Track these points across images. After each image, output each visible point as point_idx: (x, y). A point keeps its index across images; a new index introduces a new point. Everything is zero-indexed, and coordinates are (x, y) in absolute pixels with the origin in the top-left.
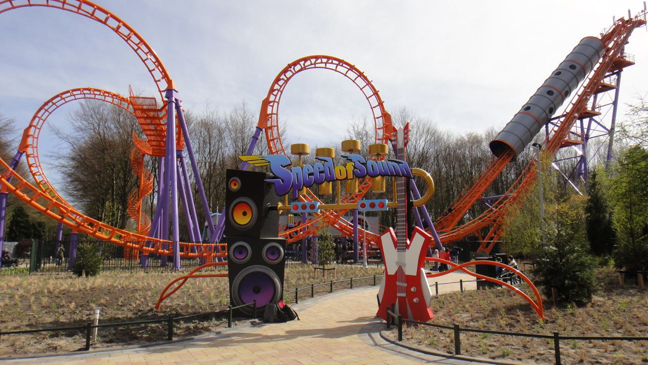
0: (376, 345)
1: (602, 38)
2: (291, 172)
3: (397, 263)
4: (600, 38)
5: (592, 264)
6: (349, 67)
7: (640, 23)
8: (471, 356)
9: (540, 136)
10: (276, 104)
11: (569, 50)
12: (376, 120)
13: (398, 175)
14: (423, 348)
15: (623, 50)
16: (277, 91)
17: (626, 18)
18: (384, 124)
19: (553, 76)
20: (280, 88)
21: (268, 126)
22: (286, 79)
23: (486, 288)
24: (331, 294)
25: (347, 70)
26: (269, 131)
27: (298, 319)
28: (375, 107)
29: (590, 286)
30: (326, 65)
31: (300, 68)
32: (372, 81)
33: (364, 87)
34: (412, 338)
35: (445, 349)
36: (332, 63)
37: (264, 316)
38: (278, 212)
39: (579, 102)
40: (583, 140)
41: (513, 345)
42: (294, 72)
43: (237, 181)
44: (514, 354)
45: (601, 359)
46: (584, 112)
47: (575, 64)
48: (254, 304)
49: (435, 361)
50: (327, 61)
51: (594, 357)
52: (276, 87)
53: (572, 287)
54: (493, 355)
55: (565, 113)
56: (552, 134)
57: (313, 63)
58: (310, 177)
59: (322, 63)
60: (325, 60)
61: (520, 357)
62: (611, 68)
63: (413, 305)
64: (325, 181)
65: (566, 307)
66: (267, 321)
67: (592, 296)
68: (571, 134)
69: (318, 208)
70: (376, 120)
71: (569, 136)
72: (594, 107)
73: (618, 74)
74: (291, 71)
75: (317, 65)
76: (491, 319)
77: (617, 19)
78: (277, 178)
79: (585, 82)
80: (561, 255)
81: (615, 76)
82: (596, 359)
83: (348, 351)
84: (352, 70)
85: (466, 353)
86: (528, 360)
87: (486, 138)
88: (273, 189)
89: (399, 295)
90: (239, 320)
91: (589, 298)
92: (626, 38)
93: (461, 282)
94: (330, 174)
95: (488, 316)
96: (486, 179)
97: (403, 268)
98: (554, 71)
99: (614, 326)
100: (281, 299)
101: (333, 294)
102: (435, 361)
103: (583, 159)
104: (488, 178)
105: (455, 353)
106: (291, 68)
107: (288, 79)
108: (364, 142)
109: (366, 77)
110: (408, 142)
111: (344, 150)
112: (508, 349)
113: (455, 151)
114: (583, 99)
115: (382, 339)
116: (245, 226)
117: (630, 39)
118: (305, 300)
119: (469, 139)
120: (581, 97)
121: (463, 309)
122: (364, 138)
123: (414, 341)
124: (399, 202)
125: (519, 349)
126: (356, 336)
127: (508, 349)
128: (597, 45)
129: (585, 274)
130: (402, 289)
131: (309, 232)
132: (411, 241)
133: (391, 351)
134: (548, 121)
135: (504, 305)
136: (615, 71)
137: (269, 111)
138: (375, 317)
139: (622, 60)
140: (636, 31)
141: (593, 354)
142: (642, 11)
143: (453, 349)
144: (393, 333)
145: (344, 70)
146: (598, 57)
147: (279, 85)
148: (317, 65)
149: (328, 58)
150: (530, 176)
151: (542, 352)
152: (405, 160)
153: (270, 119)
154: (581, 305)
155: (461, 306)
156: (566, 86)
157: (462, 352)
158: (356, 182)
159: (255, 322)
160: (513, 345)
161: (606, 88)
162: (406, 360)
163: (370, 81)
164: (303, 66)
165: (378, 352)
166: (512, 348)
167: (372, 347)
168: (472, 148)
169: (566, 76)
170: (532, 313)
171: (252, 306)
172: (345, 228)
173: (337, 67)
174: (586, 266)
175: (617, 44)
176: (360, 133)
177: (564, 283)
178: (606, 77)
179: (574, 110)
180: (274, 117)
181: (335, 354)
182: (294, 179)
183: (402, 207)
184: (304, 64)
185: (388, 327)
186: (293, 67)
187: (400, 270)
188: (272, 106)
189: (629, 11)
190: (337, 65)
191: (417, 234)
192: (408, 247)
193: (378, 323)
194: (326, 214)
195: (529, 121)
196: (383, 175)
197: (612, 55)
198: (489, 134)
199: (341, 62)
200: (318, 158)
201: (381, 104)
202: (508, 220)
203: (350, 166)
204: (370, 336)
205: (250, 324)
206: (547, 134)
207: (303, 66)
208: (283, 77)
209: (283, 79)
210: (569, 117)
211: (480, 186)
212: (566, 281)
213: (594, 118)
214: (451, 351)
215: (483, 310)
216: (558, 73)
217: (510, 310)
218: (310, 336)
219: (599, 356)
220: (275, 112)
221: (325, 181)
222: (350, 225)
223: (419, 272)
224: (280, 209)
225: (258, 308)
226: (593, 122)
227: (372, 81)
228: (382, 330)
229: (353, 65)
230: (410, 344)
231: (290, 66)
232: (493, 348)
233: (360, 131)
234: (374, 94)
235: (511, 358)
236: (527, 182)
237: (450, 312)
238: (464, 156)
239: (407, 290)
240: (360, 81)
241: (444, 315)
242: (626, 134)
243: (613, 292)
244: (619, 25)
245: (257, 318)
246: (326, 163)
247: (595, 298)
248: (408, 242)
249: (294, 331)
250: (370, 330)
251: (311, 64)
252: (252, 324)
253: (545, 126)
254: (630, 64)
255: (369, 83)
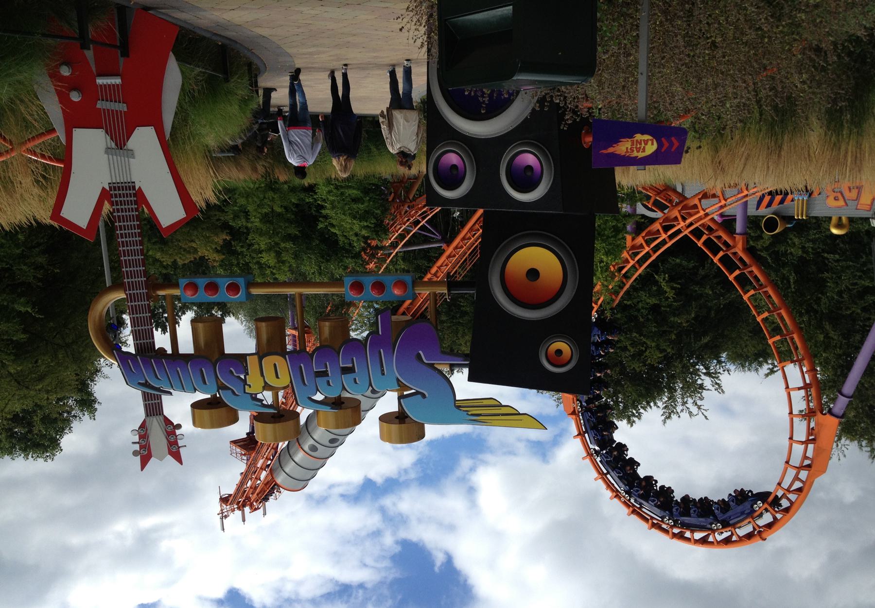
2: (398, 380)
3: (131, 154)
58: (351, 365)
77: (261, 511)
117: (238, 478)
189: (244, 520)
192: (105, 195)
254: (235, 442)
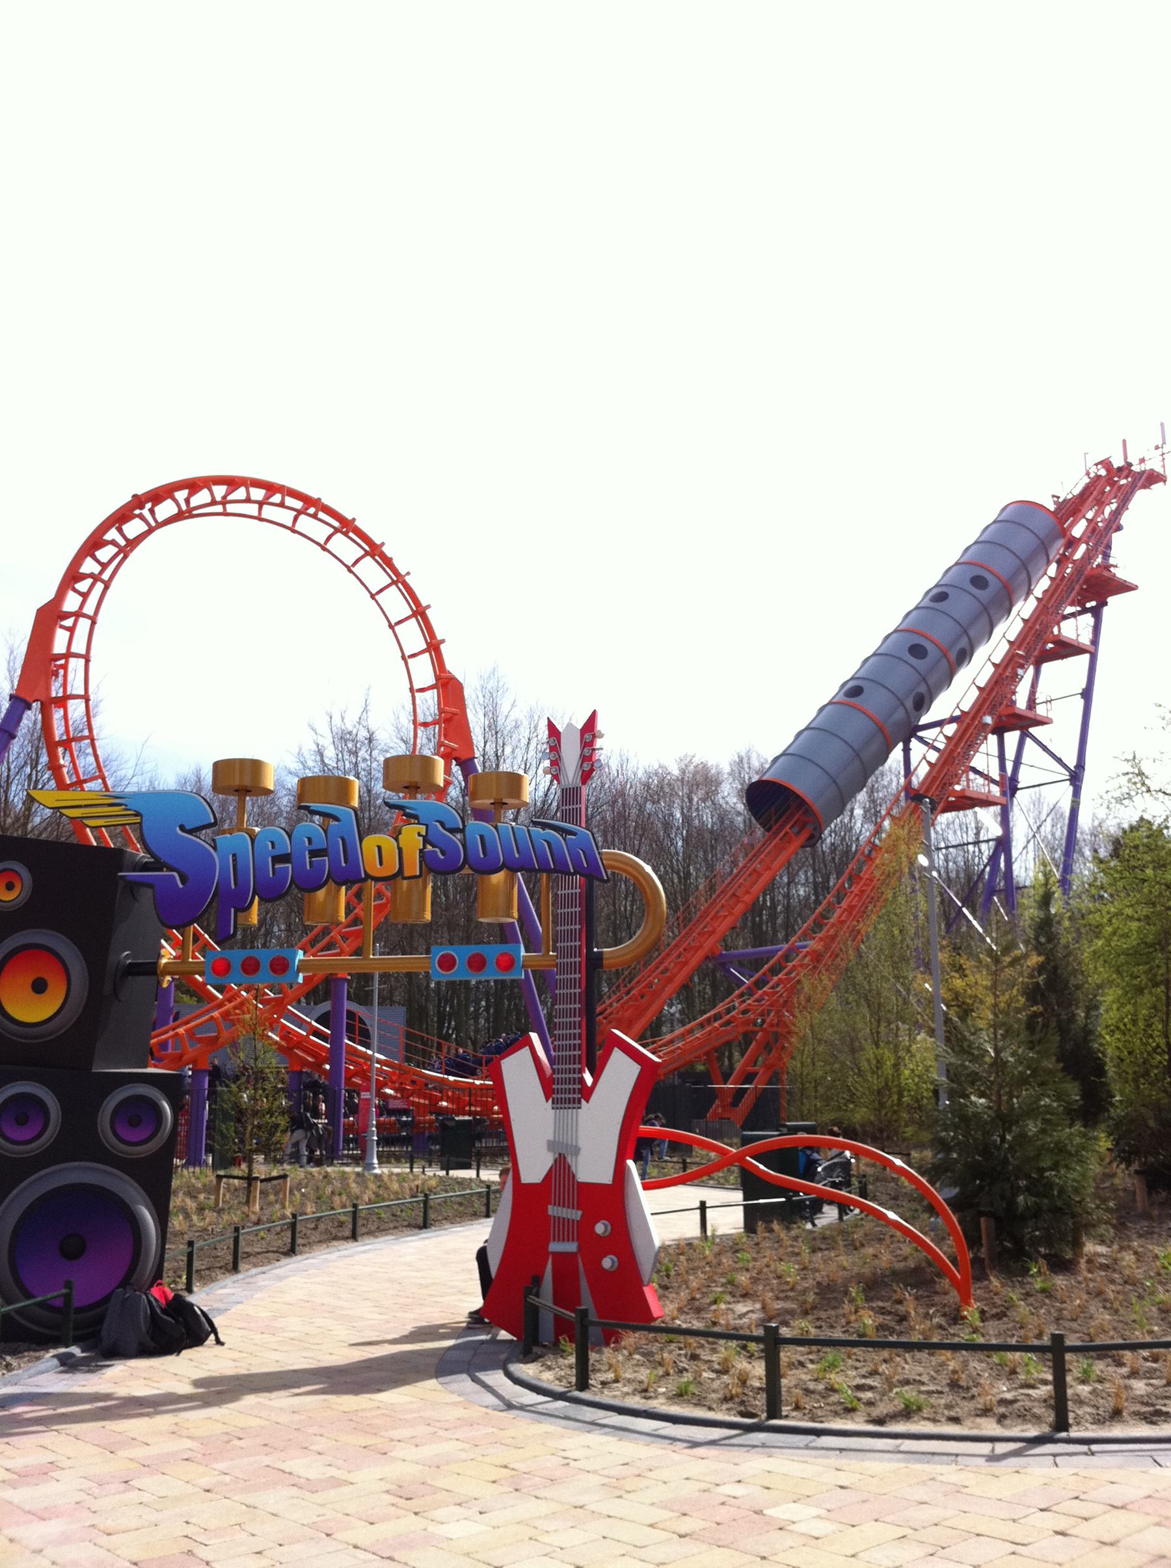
0: (510, 1406)
1: (1056, 510)
2: (215, 848)
3: (551, 1145)
4: (1052, 507)
5: (1084, 1149)
6: (336, 524)
7: (1152, 478)
8: (813, 1420)
9: (882, 774)
10: (84, 625)
11: (972, 535)
12: (417, 695)
13: (562, 869)
14: (660, 1405)
15: (1109, 547)
16: (90, 581)
17: (1118, 462)
18: (441, 711)
19: (927, 602)
20: (101, 572)
21: (54, 695)
22: (122, 543)
23: (776, 1226)
24: (425, 1234)
25: (332, 530)
26: (58, 714)
27: (219, 1342)
28: (413, 656)
29: (1079, 1210)
30: (260, 509)
31: (175, 511)
32: (408, 574)
33: (381, 591)
34: (616, 1381)
35: (730, 1405)
36: (282, 505)
37: (104, 1333)
38: (159, 983)
39: (996, 682)
40: (1003, 793)
41: (923, 1383)
42: (153, 524)
43: (18, 874)
44: (933, 1406)
45: (1165, 1405)
46: (1009, 711)
47: (987, 575)
48: (67, 1297)
49: (713, 1443)
50: (267, 497)
51: (1146, 1399)
52: (89, 566)
53: (1036, 1213)
54: (876, 1412)
55: (957, 713)
56: (922, 771)
57: (218, 499)
58: (277, 866)
59: (248, 500)
60: (258, 494)
61: (952, 1414)
62: (1078, 594)
63: (597, 1276)
64: (331, 883)
65: (1025, 1271)
66: (115, 1352)
67: (1084, 1239)
68: (972, 775)
69: (299, 970)
70: (417, 695)
71: (968, 780)
72: (1032, 703)
73: (1097, 613)
74: (141, 517)
75: (231, 508)
76: (823, 1315)
78: (157, 865)
79: (1009, 628)
80: (1005, 1120)
81: (1088, 619)
82: (1153, 1405)
83: (433, 1430)
84: (346, 534)
85: (794, 1414)
86: (978, 1420)
87: (731, 773)
88: (146, 897)
89: (554, 1247)
90: (14, 1353)
91: (1077, 1245)
92: (1117, 514)
93: (703, 1207)
94: (346, 862)
95: (814, 1308)
96: (734, 894)
97: (569, 1159)
98: (930, 590)
99: (1162, 1320)
100: (158, 1274)
101: (299, 1257)
102: (713, 1443)
103: (1003, 844)
104: (739, 893)
105: (764, 1416)
106: (142, 508)
107: (133, 543)
108: (362, 765)
109: (391, 559)
110: (592, 770)
111: (217, 787)
112: (910, 1392)
113: (641, 809)
114: (1005, 676)
115: (518, 1388)
116: (52, 1025)
117: (1125, 519)
118: (213, 1280)
119: (683, 772)
120: (1000, 670)
121: (730, 1288)
122: (363, 753)
123: (625, 1389)
124: (562, 953)
125: (941, 1393)
126: (432, 1383)
127: (910, 1392)
128: (1042, 525)
129: (1069, 1176)
130: (565, 1230)
131: (181, 1057)
132: (596, 1076)
133: (563, 1422)
134: (910, 731)
135: (845, 1273)
136: (1088, 605)
137: (59, 646)
138: (469, 1323)
139: (1105, 573)
140: (1140, 495)
141: (1138, 1392)
142: (1157, 448)
143: (760, 1403)
144: (549, 1368)
145: (319, 531)
146: (1045, 560)
147: (98, 561)
148: (231, 508)
149: (271, 488)
150: (862, 892)
151: (1009, 1396)
152: (583, 825)
153: (61, 672)
154: (1061, 1265)
155: (723, 1280)
156: (961, 635)
157: (785, 1410)
158: (425, 888)
159: (72, 1355)
160: (923, 1383)
161: (1066, 649)
162: (623, 1443)
163: (403, 572)
164: (184, 507)
165: (523, 1427)
166: (920, 1392)
167: (501, 1414)
168: (691, 800)
169: (962, 605)
170: (936, 1293)
171: (59, 1303)
172: (301, 1043)
173: (296, 519)
174: (1070, 1154)
175: (1094, 530)
176: (350, 733)
177: (1012, 1203)
178: (1065, 617)
179: (982, 705)
180: (76, 665)
181: (392, 1440)
182: (224, 871)
183: (571, 968)
184: (187, 501)
185: (529, 1349)
186: (149, 505)
187: (561, 1168)
188: (71, 630)
190: (299, 512)
191: (617, 1055)
192: (586, 1093)
193: (482, 1342)
194: (238, 994)
195: (857, 727)
196: (512, 867)
197: (1083, 557)
198: (741, 761)
199: (311, 504)
200: (307, 808)
201: (434, 647)
202: (801, 1023)
203: (412, 836)
204: (476, 1380)
205: (55, 1362)
206: (908, 772)
207: (184, 507)
208: (112, 534)
209: (113, 543)
210: (969, 725)
211: (715, 917)
212: (1021, 1198)
213: (1032, 730)
214: (751, 1409)
215: (792, 1289)
216: (939, 596)
217: (874, 1286)
218: (283, 1393)
219: (1157, 1398)
220: (79, 647)
221: (331, 883)
222: (317, 1033)
223: (620, 1171)
224: (166, 972)
225: (79, 1310)
226: (1028, 741)
227: (408, 574)
228: (509, 1360)
229: (350, 517)
230: (615, 1397)
231: (138, 501)
232: (869, 1395)
233: (350, 729)
234: (414, 614)
235: (928, 1419)
236: (851, 908)
237: (693, 1299)
238: (667, 826)
239: (583, 1230)
240: (371, 571)
241: (680, 1310)
242: (1143, 784)
243: (1127, 1228)
244: (1098, 477)
245: (76, 1341)
246: (333, 823)
247: (1091, 1247)
248: (588, 1079)
249: (216, 1378)
250: (469, 1363)
251: (214, 502)
252: (62, 1364)
253: (900, 745)
254: (1125, 587)
255: (399, 580)
